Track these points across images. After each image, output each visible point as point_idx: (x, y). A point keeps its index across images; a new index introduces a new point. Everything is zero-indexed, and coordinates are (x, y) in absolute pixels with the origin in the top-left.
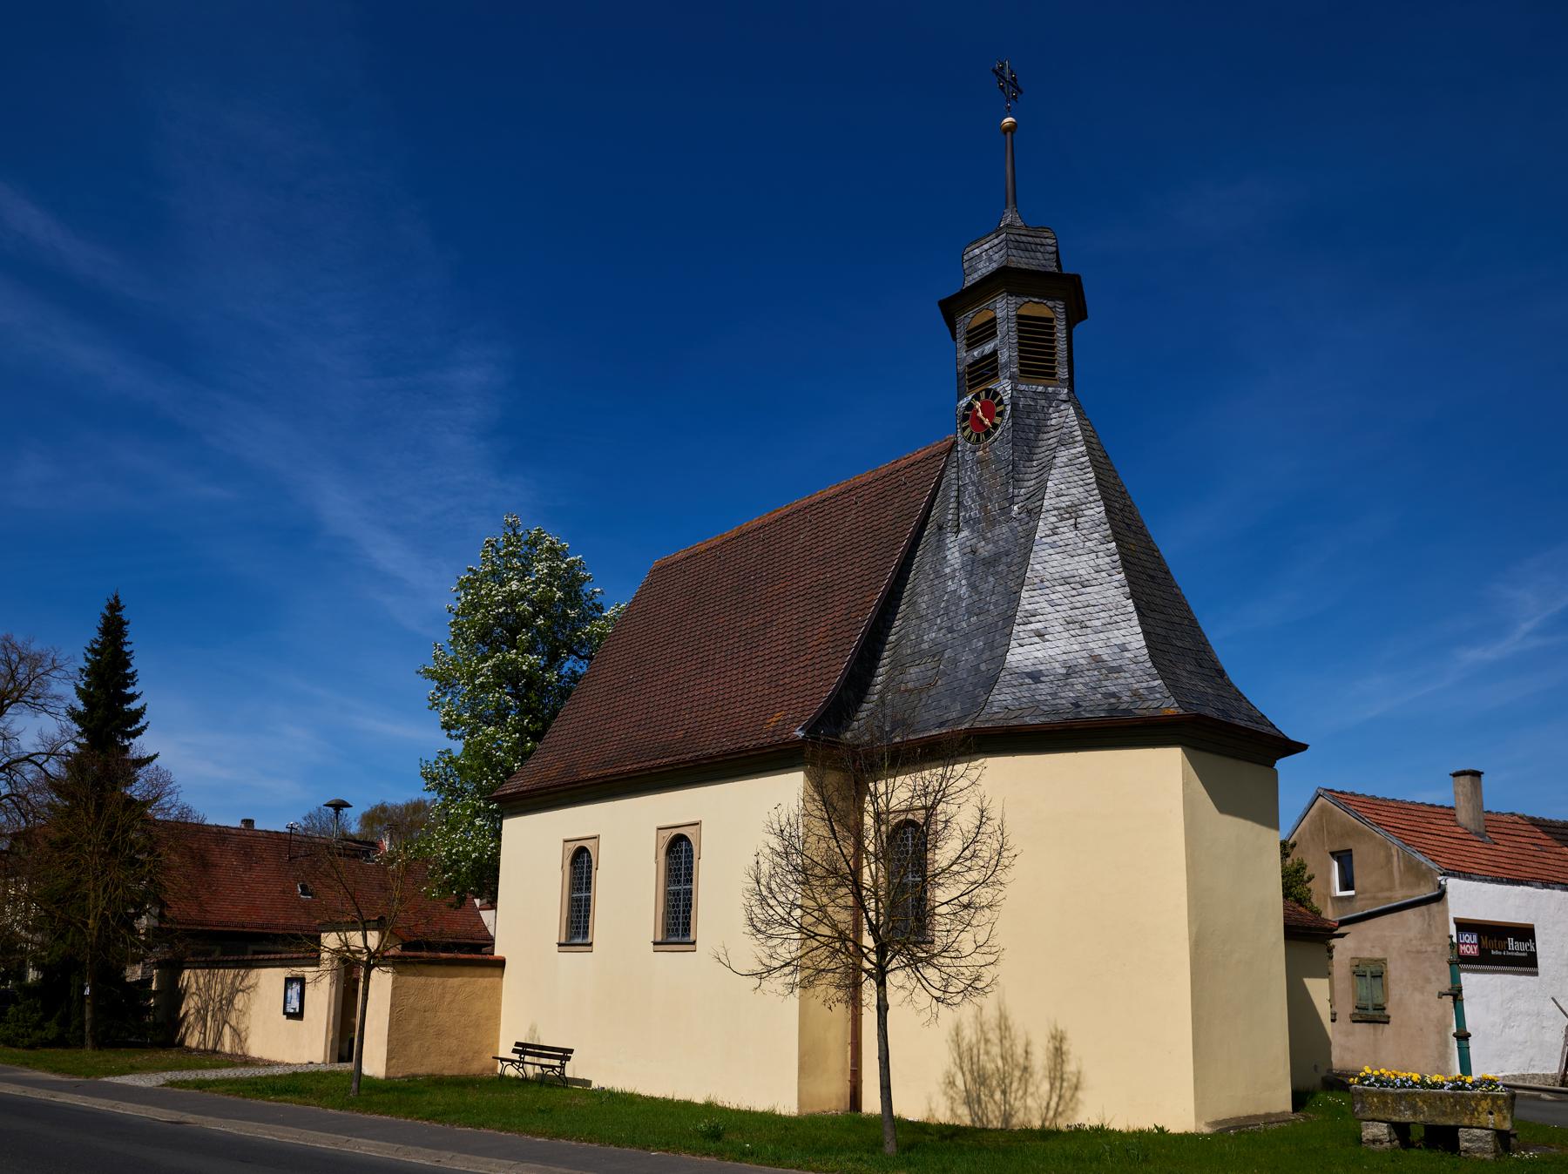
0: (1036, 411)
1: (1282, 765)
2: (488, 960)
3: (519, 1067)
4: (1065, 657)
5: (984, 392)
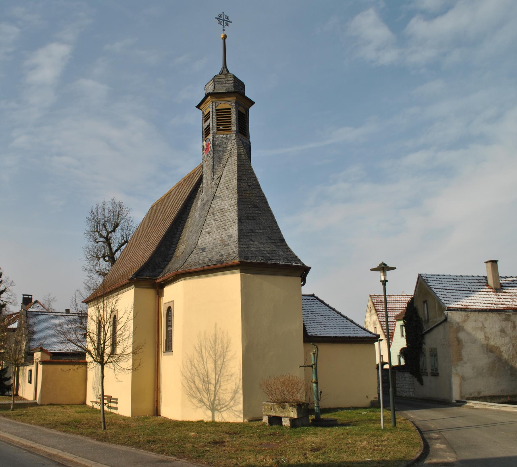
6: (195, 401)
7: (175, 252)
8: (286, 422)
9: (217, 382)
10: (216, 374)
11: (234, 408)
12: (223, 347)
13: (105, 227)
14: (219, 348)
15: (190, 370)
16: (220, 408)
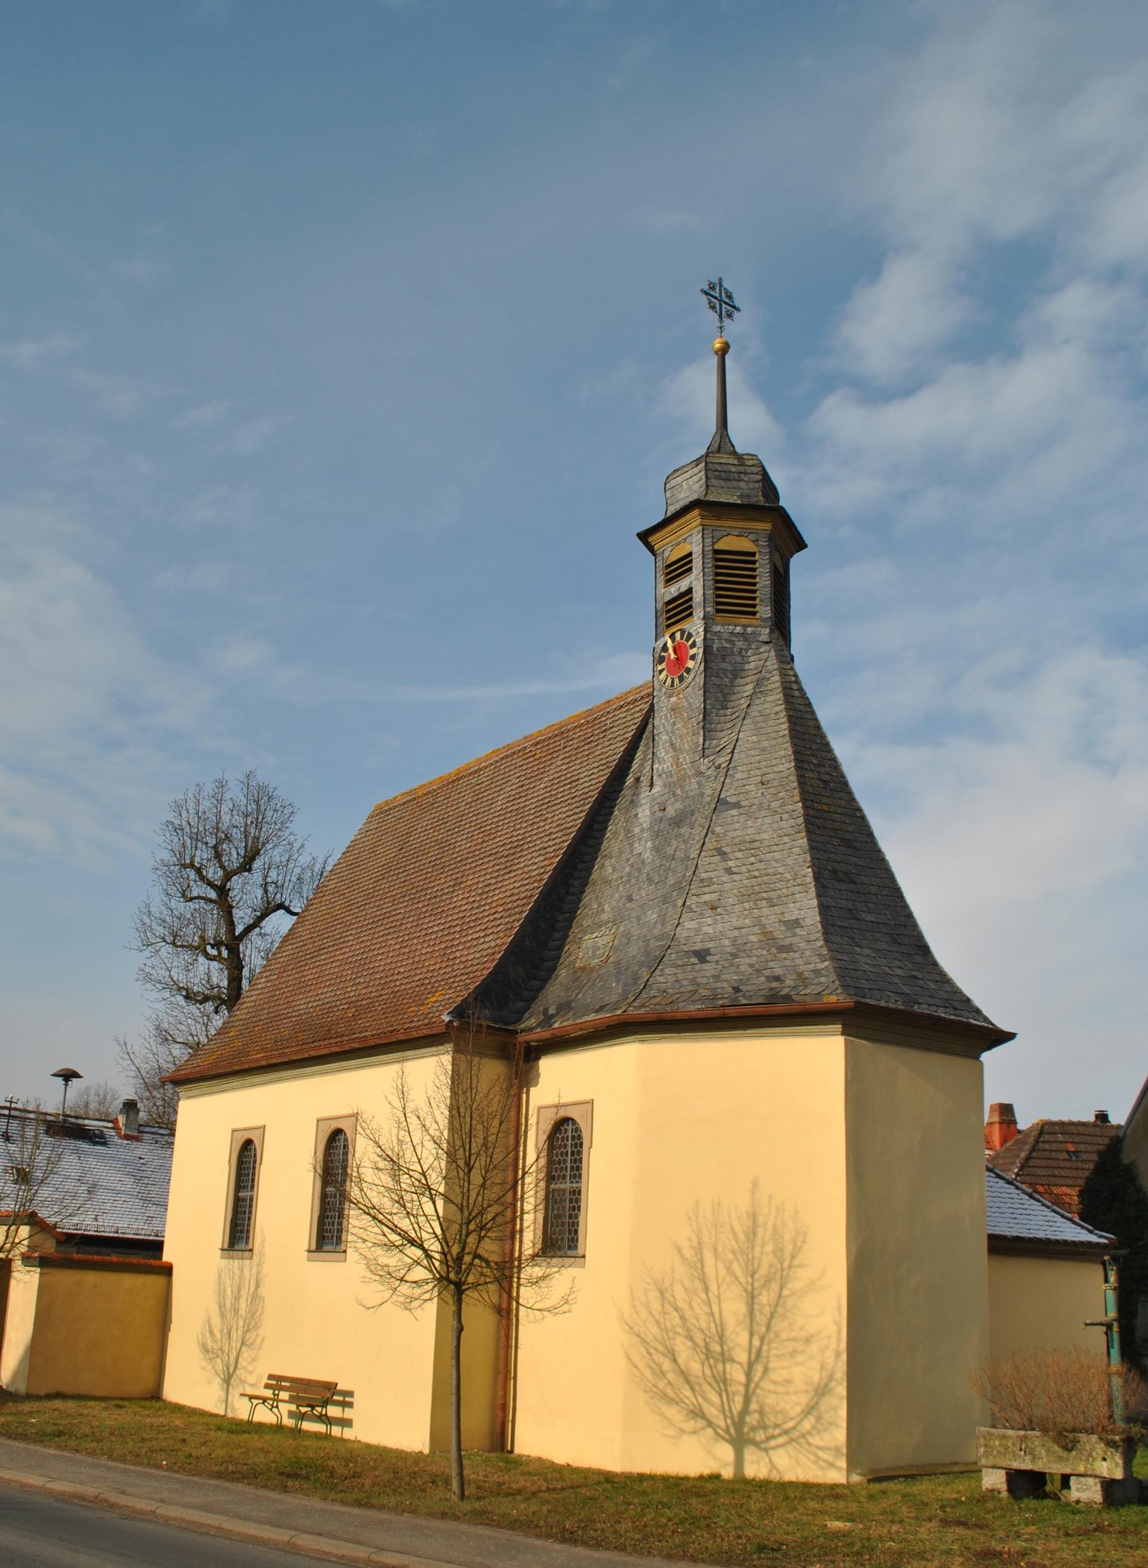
0: (733, 653)
1: (990, 1058)
2: (152, 1266)
3: (273, 1407)
4: (736, 933)
5: (679, 633)
6: (674, 1413)
7: (564, 956)
8: (1084, 1491)
9: (756, 1357)
10: (752, 1334)
11: (815, 1440)
12: (778, 1252)
13: (218, 855)
14: (764, 1255)
15: (657, 1317)
16: (763, 1437)
